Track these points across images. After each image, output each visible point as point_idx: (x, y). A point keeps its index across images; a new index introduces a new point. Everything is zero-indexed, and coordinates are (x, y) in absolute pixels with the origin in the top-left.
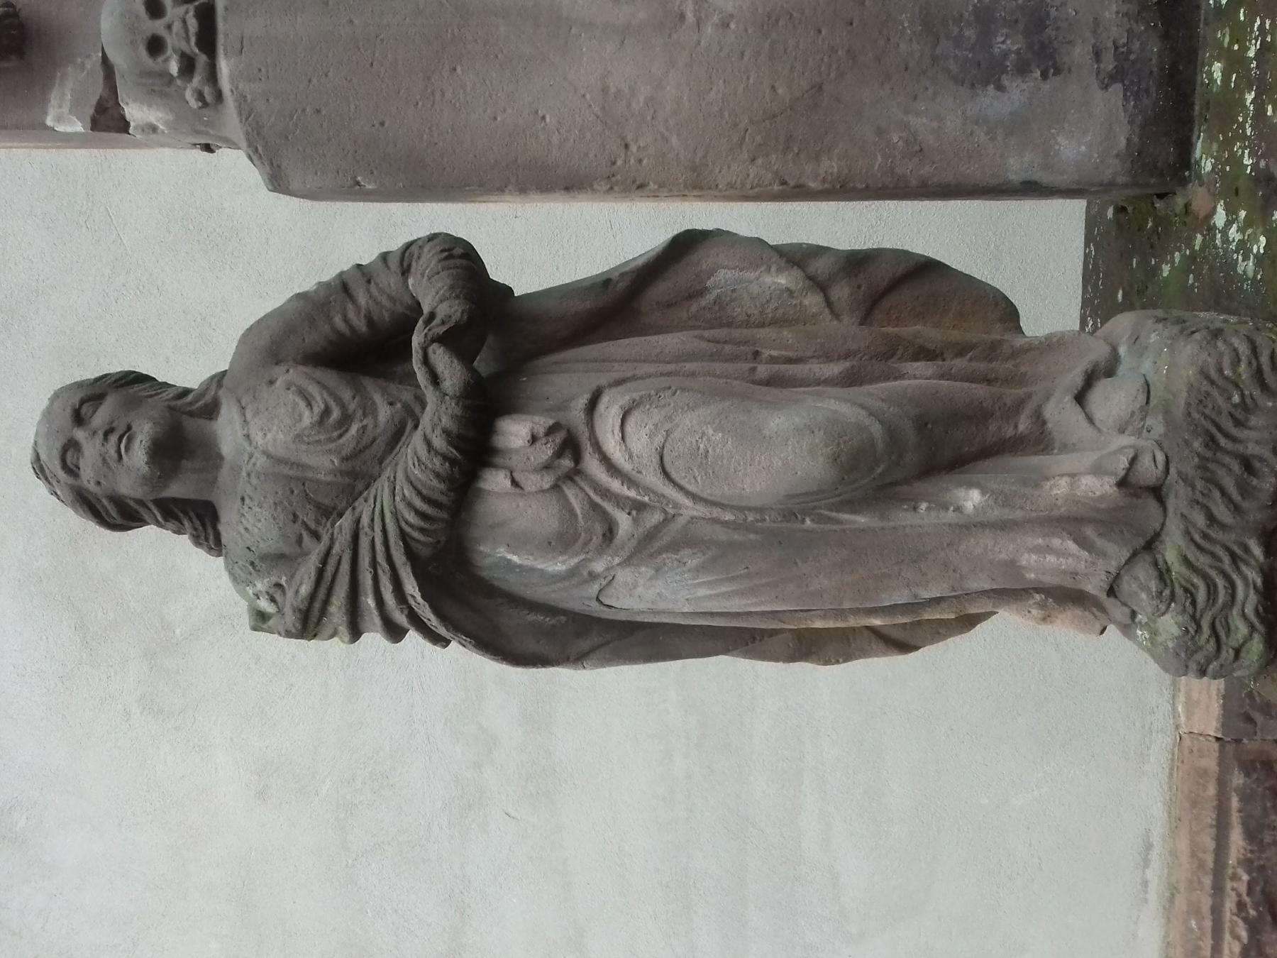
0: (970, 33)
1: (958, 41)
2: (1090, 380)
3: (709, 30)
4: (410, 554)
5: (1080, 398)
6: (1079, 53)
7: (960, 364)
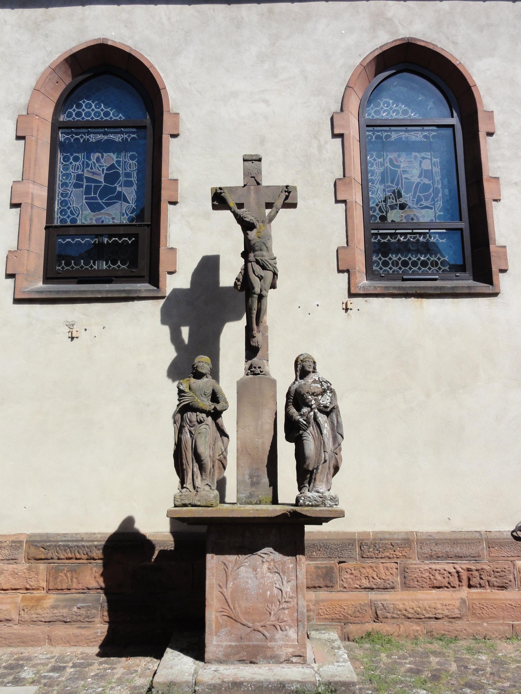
0: (256, 474)
1: (255, 473)
2: (210, 486)
3: (257, 440)
4: (189, 403)
5: (207, 484)
6: (254, 489)
7: (212, 470)
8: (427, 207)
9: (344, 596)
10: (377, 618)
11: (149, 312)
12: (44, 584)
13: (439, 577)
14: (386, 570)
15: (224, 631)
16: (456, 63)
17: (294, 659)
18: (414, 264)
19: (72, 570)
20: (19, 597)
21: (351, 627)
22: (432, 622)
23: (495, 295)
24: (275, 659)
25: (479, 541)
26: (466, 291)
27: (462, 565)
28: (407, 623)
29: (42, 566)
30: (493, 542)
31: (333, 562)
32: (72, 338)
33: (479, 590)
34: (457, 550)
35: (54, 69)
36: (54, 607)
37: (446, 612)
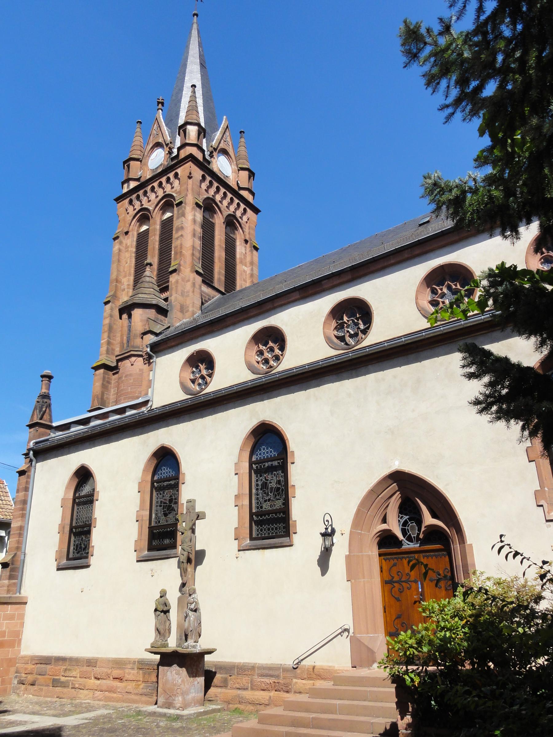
8: (279, 499)
9: (230, 691)
10: (240, 703)
11: (174, 562)
12: (141, 679)
13: (263, 685)
14: (245, 681)
15: (163, 695)
16: (280, 429)
17: (180, 709)
18: (276, 529)
19: (149, 674)
20: (134, 684)
21: (231, 706)
22: (258, 706)
23: (292, 545)
24: (174, 708)
25: (279, 668)
26: (279, 545)
27: (272, 680)
28: (249, 705)
29: (141, 672)
30: (285, 670)
31: (227, 676)
32: (342, 534)
33: (279, 693)
34: (271, 672)
35: (149, 460)
36: (143, 689)
37: (263, 702)
